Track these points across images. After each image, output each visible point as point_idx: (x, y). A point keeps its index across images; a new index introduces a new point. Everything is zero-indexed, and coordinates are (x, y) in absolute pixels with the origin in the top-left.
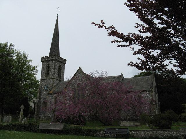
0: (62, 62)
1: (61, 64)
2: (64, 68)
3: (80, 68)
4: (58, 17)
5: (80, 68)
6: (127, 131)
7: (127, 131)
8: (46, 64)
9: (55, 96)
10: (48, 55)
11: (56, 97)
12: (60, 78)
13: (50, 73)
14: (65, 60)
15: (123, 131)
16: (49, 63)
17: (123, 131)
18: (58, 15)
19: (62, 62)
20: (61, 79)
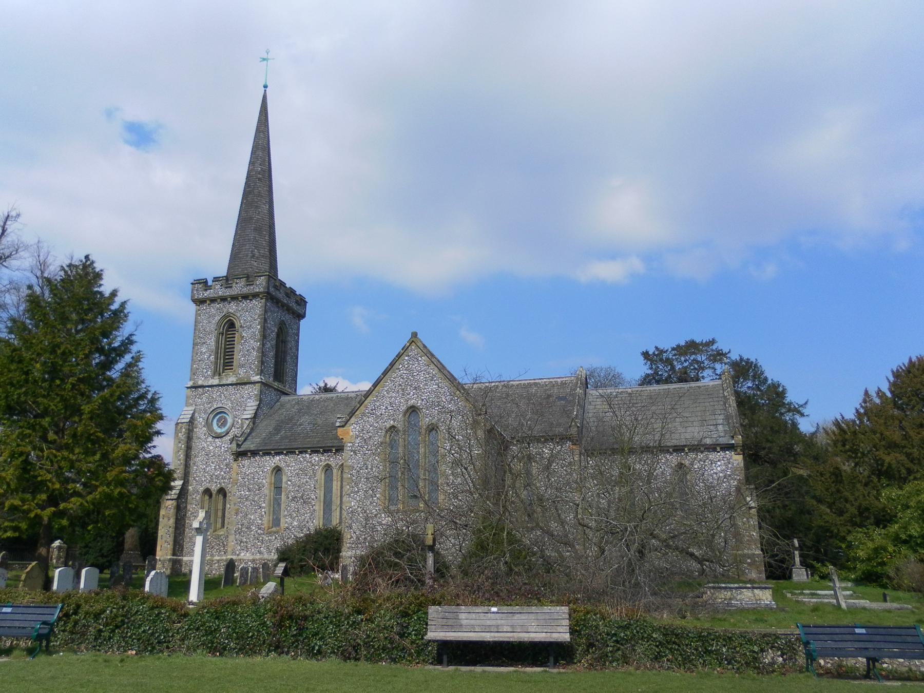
0: (289, 310)
1: (288, 318)
2: (298, 335)
4: (265, 91)
8: (215, 313)
13: (238, 357)
16: (232, 307)
19: (289, 310)
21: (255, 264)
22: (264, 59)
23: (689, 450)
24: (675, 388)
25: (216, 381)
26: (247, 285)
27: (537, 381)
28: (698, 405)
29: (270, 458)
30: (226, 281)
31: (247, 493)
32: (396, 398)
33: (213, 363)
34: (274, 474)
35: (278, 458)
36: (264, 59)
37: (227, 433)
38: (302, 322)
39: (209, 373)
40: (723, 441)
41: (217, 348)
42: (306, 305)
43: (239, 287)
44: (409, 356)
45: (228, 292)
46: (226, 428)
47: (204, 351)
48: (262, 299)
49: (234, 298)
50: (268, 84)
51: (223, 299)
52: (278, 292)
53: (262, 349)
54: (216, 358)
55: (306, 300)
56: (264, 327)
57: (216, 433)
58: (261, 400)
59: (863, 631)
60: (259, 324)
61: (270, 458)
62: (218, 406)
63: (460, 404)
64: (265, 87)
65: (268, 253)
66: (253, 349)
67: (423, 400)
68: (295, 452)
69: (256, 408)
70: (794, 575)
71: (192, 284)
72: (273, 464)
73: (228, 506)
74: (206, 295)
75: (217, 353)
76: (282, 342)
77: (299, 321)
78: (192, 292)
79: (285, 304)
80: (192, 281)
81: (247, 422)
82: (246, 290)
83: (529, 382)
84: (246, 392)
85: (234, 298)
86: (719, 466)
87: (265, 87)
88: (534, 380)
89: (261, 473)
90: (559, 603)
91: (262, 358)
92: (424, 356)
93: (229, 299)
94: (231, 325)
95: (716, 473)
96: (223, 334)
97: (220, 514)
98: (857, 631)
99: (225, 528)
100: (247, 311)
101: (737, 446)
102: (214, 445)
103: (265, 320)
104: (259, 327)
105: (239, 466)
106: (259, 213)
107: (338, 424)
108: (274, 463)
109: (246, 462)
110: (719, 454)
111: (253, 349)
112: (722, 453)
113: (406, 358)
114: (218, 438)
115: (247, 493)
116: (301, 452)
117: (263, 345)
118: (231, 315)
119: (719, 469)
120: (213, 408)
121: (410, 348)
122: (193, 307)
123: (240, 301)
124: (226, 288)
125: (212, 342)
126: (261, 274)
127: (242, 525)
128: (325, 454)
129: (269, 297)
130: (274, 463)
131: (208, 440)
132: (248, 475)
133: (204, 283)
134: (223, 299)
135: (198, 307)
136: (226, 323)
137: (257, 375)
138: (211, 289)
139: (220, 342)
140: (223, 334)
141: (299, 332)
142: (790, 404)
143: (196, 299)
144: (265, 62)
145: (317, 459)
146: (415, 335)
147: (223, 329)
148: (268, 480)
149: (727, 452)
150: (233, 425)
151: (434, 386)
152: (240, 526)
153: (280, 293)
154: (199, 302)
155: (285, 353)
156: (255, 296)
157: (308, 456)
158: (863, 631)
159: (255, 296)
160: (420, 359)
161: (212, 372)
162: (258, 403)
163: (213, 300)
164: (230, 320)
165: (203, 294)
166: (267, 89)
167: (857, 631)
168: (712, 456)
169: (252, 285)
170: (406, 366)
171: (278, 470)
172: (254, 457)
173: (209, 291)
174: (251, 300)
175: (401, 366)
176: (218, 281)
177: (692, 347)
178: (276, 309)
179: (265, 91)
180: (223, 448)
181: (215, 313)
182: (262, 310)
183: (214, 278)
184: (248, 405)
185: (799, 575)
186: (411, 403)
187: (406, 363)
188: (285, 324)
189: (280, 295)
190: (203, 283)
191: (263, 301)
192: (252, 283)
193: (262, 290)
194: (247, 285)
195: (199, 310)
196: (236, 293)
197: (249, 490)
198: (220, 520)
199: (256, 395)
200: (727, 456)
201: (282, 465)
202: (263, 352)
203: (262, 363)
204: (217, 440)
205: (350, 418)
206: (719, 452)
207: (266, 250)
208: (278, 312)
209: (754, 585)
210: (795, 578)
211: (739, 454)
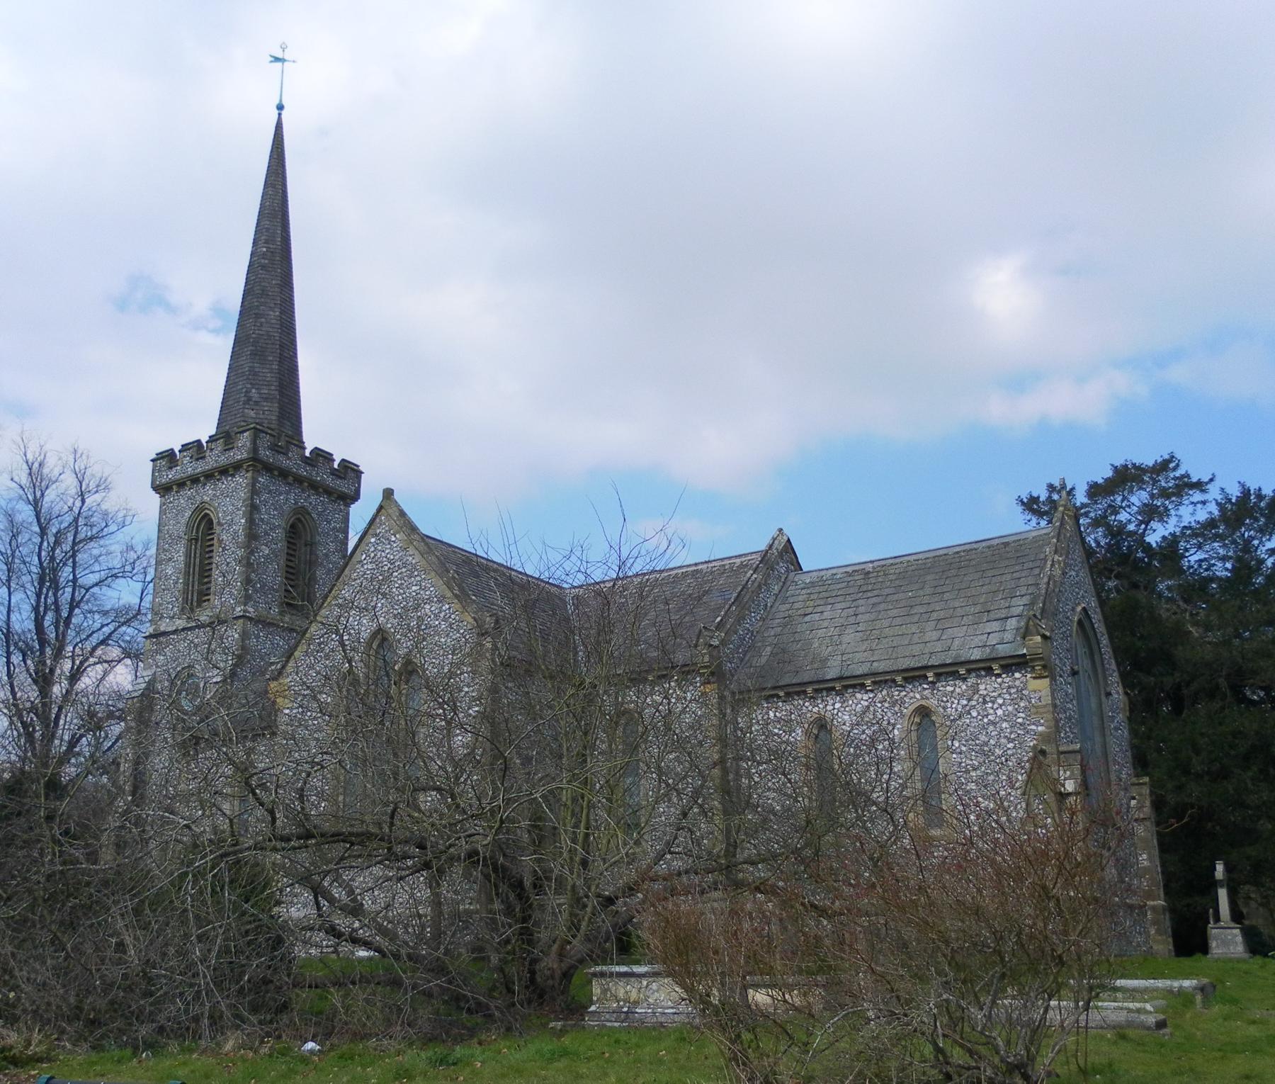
1: (314, 502)
4: (280, 114)
8: (185, 502)
16: (207, 493)
21: (252, 413)
22: (277, 59)
23: (938, 675)
24: (958, 553)
26: (225, 450)
27: (700, 567)
28: (987, 581)
36: (277, 59)
39: (176, 609)
40: (1004, 650)
41: (188, 565)
44: (376, 535)
47: (170, 572)
48: (247, 471)
49: (209, 476)
50: (284, 103)
51: (195, 480)
52: (281, 457)
55: (361, 468)
63: (453, 616)
64: (280, 107)
65: (277, 393)
70: (1214, 944)
71: (152, 460)
74: (170, 476)
77: (348, 505)
78: (153, 475)
79: (305, 477)
80: (154, 456)
82: (223, 460)
83: (684, 570)
85: (209, 476)
86: (1001, 706)
87: (280, 107)
88: (696, 564)
92: (399, 532)
93: (202, 479)
95: (994, 723)
96: (196, 540)
100: (228, 496)
101: (1032, 660)
104: (243, 521)
106: (261, 326)
110: (999, 680)
112: (1007, 679)
113: (373, 540)
118: (207, 506)
119: (1000, 712)
121: (378, 520)
122: (156, 498)
123: (218, 480)
124: (197, 460)
125: (180, 556)
126: (244, 428)
134: (195, 480)
138: (177, 466)
139: (193, 555)
141: (347, 527)
142: (321, 456)
143: (159, 486)
144: (279, 64)
146: (781, 530)
147: (197, 532)
149: (1017, 675)
151: (414, 588)
156: (237, 467)
159: (237, 467)
160: (393, 539)
163: (181, 484)
166: (284, 113)
168: (987, 686)
169: (233, 448)
170: (372, 555)
173: (174, 469)
174: (233, 476)
175: (364, 556)
176: (189, 449)
177: (1125, 477)
178: (283, 488)
179: (280, 114)
182: (248, 492)
185: (1225, 943)
187: (372, 549)
188: (309, 514)
192: (230, 446)
193: (245, 455)
194: (225, 450)
195: (164, 504)
196: (210, 467)
200: (1017, 683)
205: (287, 661)
206: (999, 676)
207: (273, 388)
208: (288, 493)
210: (1216, 948)
211: (1041, 677)
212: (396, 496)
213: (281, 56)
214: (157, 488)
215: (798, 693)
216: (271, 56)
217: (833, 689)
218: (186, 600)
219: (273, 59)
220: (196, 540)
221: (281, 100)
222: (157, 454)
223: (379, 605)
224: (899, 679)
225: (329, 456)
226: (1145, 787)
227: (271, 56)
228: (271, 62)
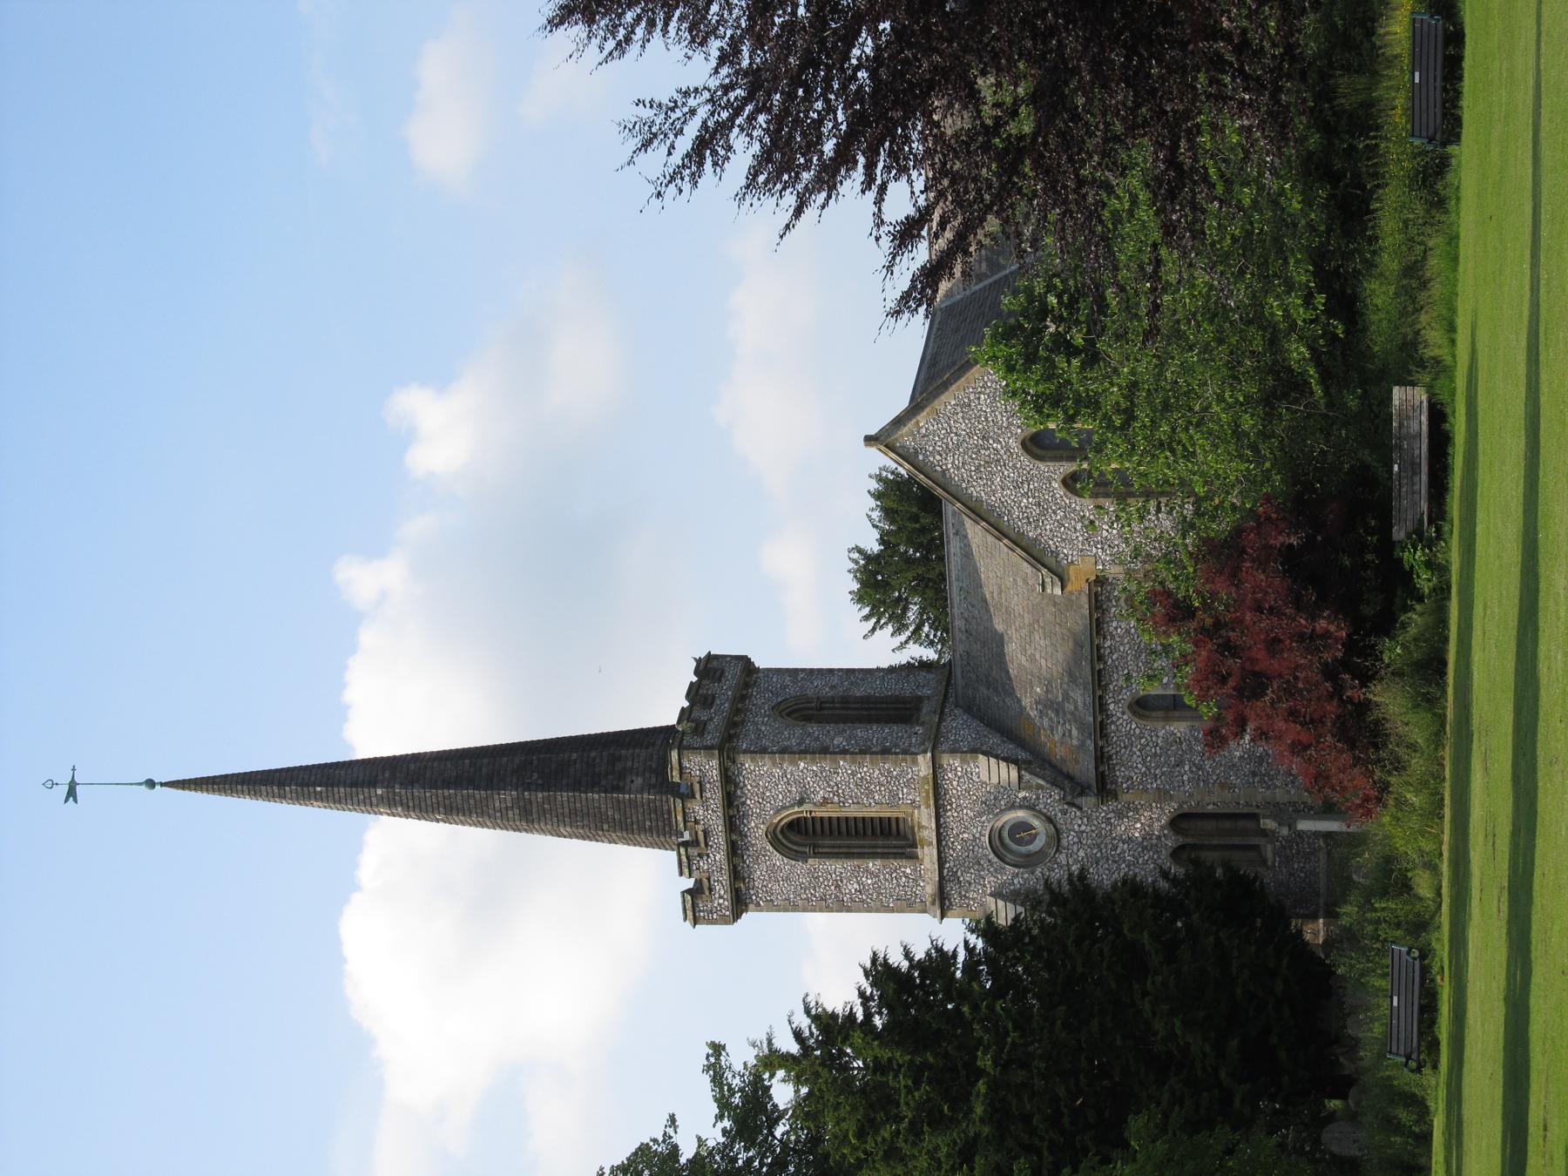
0: (742, 697)
1: (760, 700)
2: (795, 672)
3: (869, 440)
4: (162, 784)
5: (869, 440)
6: (1425, 26)
7: (1425, 26)
8: (768, 864)
9: (1122, 721)
10: (669, 858)
11: (1142, 707)
12: (918, 709)
13: (872, 809)
14: (709, 668)
15: (1424, 120)
16: (756, 831)
17: (1424, 120)
18: (151, 784)
19: (742, 697)
20: (920, 699)
22: (72, 793)
25: (928, 855)
29: (1113, 722)
30: (691, 852)
31: (1187, 768)
32: (1004, 477)
33: (886, 862)
34: (1147, 713)
35: (1112, 707)
36: (72, 793)
37: (1049, 820)
38: (761, 662)
42: (717, 657)
43: (708, 812)
45: (719, 839)
46: (1036, 823)
47: (856, 886)
52: (711, 727)
53: (852, 753)
54: (873, 856)
56: (801, 752)
57: (1047, 844)
58: (975, 751)
59: (1417, 74)
60: (794, 763)
61: (1113, 722)
62: (987, 836)
66: (854, 774)
67: (1010, 424)
68: (1100, 671)
69: (993, 760)
72: (1125, 717)
73: (1210, 807)
75: (861, 856)
76: (821, 709)
81: (1027, 776)
82: (715, 796)
84: (955, 783)
89: (1143, 741)
90: (1391, 392)
91: (876, 753)
94: (796, 826)
97: (1227, 824)
98: (1417, 81)
99: (1257, 811)
102: (1075, 848)
103: (783, 751)
105: (1128, 788)
107: (1058, 591)
108: (1123, 713)
109: (1120, 773)
111: (854, 774)
113: (921, 457)
114: (1059, 840)
115: (1187, 768)
116: (1100, 658)
117: (844, 752)
120: (992, 856)
127: (1254, 774)
128: (1105, 607)
129: (727, 749)
130: (1123, 713)
131: (1064, 862)
132: (1148, 769)
133: (694, 894)
135: (751, 906)
136: (791, 842)
137: (915, 762)
140: (815, 846)
145: (1114, 624)
147: (805, 846)
148: (1159, 725)
150: (1031, 807)
152: (1256, 779)
153: (711, 719)
154: (740, 904)
155: (846, 701)
156: (730, 783)
157: (1108, 643)
158: (1417, 74)
159: (730, 783)
161: (904, 862)
162: (981, 756)
164: (782, 831)
165: (721, 897)
167: (1417, 81)
170: (938, 457)
171: (1142, 707)
172: (1110, 758)
179: (162, 784)
180: (1083, 828)
181: (768, 864)
183: (681, 874)
184: (984, 777)
186: (1014, 445)
189: (716, 720)
190: (696, 904)
191: (741, 758)
193: (715, 763)
197: (1180, 764)
198: (1241, 824)
199: (964, 761)
201: (1126, 696)
202: (862, 752)
203: (885, 751)
204: (1064, 842)
209: (1318, 925)
212: (873, 432)
213: (67, 787)
214: (736, 916)
215: (1099, 677)
216: (66, 801)
217: (1100, 697)
218: (896, 856)
219: (71, 799)
220: (815, 846)
221: (140, 784)
222: (685, 919)
223: (995, 445)
224: (1099, 693)
225: (694, 688)
226: (953, 785)
227: (66, 801)
228: (75, 801)
